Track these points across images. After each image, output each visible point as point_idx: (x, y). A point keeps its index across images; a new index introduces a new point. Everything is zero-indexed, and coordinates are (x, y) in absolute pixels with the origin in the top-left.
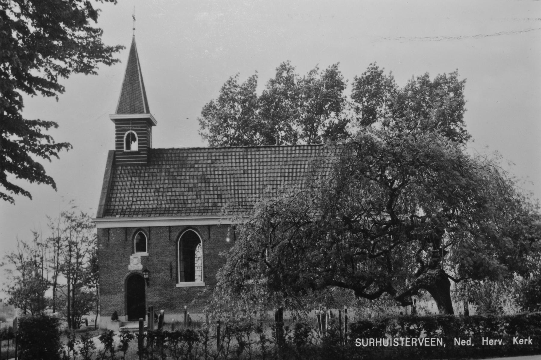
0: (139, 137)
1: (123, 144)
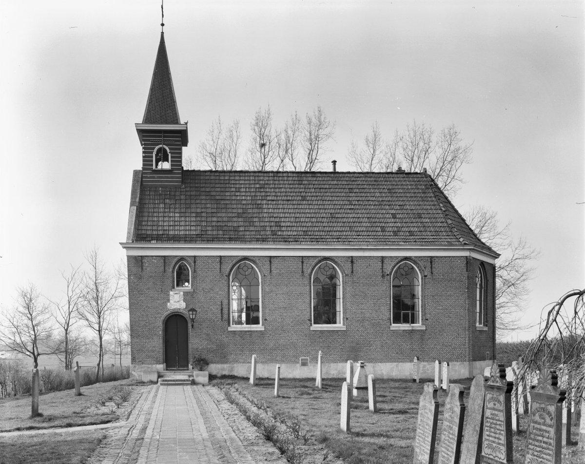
0: (172, 157)
1: (152, 161)
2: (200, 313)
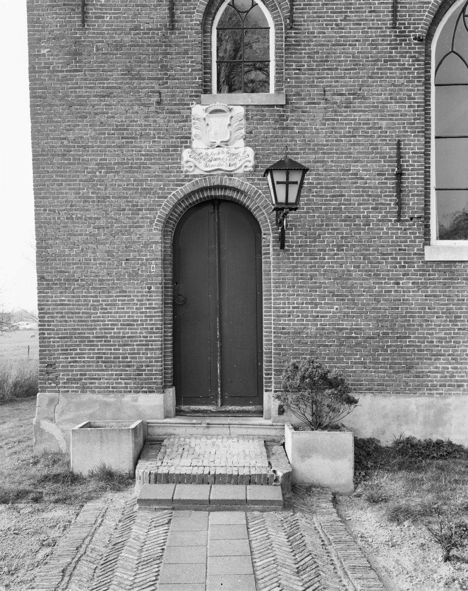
2: (310, 190)
